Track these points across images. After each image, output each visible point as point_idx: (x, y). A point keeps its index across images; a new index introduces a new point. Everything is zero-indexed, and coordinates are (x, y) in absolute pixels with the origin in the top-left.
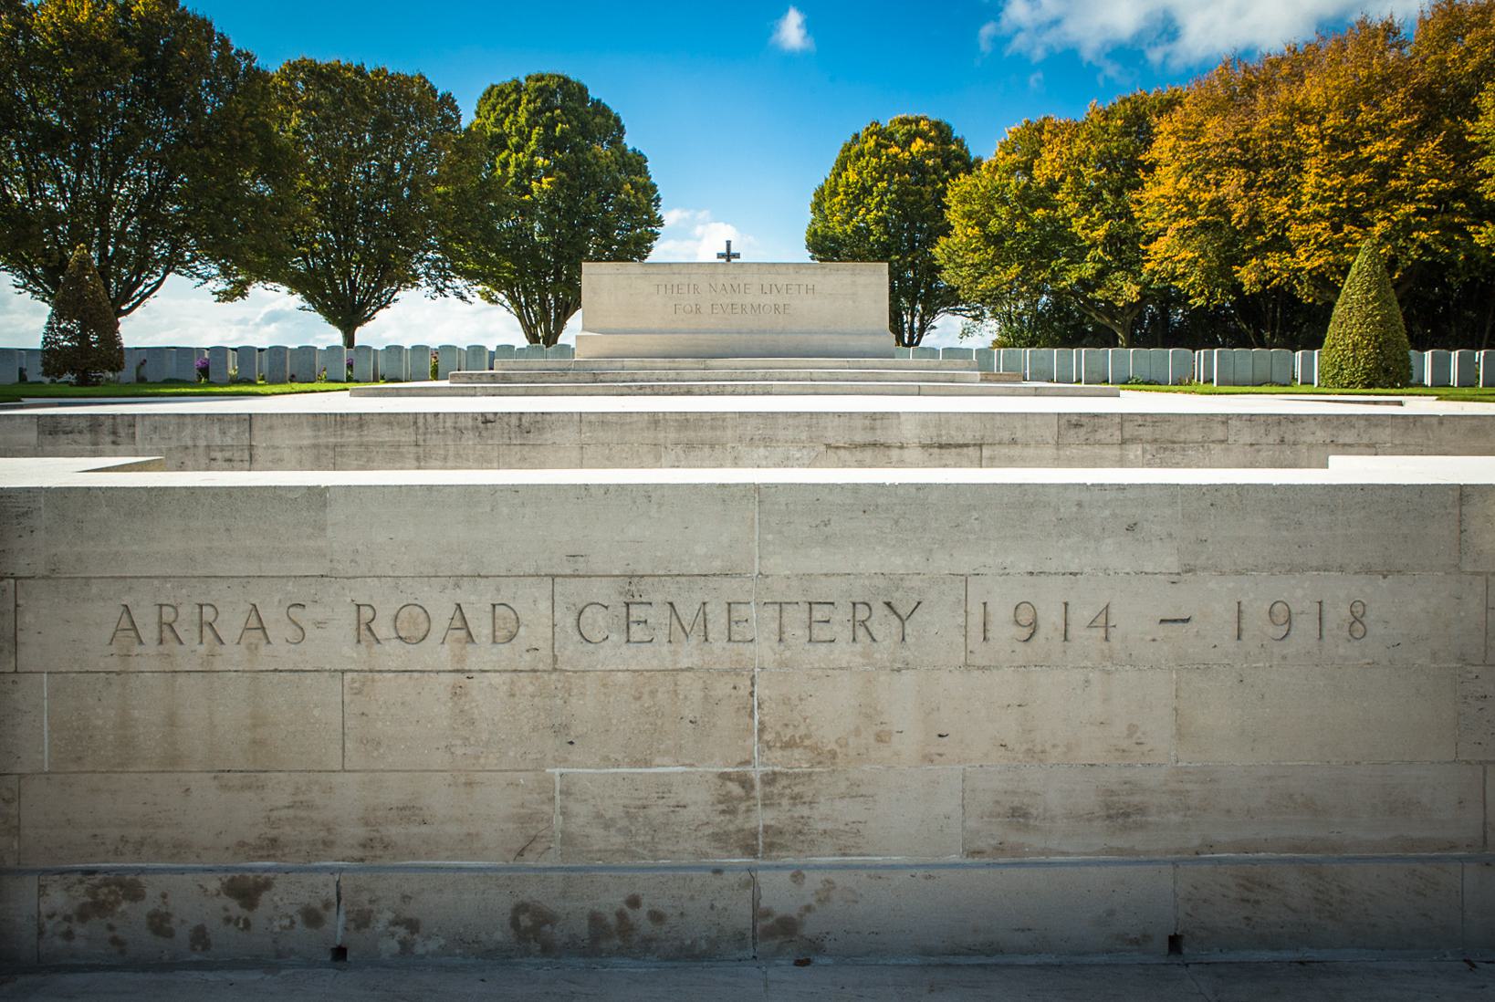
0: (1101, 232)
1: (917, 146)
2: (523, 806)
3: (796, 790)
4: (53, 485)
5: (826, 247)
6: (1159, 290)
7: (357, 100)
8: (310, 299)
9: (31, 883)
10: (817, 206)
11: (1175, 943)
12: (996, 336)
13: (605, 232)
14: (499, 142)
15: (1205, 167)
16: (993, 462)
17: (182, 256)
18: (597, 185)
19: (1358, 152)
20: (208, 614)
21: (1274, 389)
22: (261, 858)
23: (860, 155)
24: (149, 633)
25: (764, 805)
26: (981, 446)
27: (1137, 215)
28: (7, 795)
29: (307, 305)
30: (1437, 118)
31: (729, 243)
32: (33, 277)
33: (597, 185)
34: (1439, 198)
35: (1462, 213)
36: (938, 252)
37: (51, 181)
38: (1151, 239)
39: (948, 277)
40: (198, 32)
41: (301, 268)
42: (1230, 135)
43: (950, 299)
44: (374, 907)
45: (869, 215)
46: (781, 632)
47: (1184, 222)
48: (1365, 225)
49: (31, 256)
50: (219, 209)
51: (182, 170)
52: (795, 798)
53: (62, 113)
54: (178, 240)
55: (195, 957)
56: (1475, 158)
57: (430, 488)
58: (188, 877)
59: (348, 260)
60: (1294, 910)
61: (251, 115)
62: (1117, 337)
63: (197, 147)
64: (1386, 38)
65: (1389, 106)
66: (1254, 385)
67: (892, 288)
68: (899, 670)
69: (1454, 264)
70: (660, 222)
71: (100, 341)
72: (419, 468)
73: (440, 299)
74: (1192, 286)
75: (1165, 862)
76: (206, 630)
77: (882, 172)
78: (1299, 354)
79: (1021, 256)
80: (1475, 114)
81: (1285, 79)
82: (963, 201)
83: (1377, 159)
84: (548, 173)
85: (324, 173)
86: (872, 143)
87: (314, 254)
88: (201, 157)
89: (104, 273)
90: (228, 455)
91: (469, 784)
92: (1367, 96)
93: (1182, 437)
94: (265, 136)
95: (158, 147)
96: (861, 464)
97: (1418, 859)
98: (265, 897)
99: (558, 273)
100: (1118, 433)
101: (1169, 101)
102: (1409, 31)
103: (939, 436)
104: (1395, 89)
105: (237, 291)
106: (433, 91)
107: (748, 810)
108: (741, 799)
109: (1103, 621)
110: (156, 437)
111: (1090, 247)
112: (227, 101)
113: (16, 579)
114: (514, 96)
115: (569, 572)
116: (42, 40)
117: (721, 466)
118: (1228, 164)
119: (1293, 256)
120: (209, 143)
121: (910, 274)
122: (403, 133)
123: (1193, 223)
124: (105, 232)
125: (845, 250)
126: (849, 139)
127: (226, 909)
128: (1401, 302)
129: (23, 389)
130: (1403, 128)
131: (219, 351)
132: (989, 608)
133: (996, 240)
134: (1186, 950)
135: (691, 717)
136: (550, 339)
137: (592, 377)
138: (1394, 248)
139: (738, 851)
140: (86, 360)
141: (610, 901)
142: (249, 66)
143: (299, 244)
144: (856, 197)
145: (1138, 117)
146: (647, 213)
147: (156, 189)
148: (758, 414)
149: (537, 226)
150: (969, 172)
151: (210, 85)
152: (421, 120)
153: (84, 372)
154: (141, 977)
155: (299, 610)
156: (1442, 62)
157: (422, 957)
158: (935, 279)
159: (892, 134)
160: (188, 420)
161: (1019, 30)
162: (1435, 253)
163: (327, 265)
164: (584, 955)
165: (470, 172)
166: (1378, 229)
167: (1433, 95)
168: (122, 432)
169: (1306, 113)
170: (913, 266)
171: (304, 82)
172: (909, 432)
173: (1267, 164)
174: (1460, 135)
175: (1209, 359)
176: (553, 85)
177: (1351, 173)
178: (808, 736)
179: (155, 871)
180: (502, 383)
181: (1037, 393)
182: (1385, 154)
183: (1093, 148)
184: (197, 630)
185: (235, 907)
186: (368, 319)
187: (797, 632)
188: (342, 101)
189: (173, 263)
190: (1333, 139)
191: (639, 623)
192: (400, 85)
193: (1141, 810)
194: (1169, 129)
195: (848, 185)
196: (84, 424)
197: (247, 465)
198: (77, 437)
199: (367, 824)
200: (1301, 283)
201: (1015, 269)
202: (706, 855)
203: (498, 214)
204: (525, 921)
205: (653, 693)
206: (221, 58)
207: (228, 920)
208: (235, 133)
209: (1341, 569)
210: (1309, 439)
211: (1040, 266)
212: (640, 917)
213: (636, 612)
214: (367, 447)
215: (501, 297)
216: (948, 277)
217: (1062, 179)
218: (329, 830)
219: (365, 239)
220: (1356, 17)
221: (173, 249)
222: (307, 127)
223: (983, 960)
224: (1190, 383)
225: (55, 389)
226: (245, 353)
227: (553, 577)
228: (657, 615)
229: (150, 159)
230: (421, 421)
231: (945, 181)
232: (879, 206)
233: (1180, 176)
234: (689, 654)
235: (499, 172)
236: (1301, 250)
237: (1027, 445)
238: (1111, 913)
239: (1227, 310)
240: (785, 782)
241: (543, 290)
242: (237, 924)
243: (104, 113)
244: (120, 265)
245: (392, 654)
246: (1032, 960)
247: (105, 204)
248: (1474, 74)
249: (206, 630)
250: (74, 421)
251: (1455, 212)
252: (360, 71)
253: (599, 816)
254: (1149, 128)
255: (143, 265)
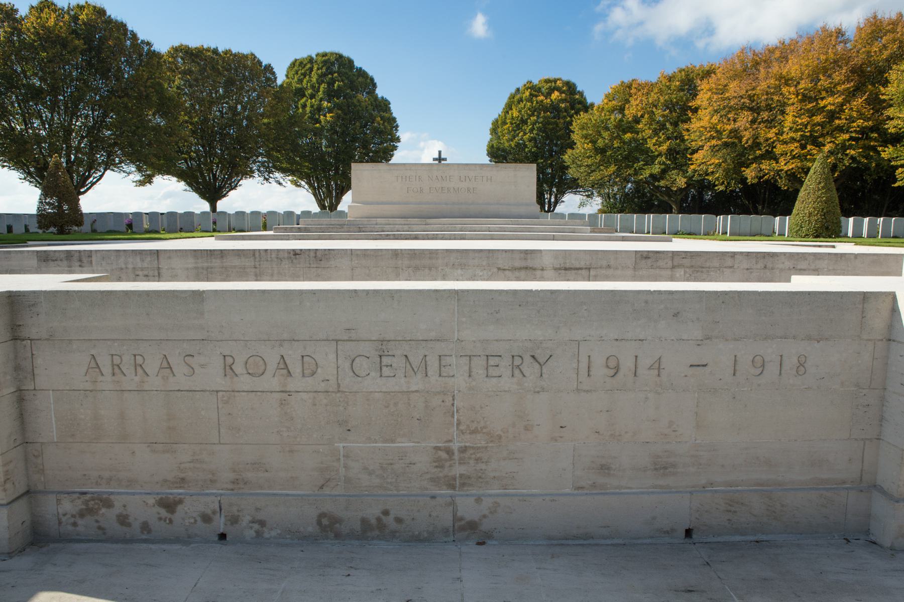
0: (664, 148)
1: (555, 95)
2: (322, 463)
3: (478, 456)
4: (44, 289)
5: (498, 154)
6: (698, 181)
7: (214, 68)
8: (189, 184)
9: (52, 498)
10: (494, 131)
11: (688, 533)
12: (600, 207)
13: (365, 145)
14: (300, 93)
15: (727, 110)
16: (596, 278)
17: (114, 161)
18: (360, 118)
19: (818, 103)
20: (139, 360)
21: (762, 238)
22: (177, 488)
23: (521, 100)
24: (107, 369)
25: (460, 463)
26: (589, 269)
27: (686, 137)
28: (36, 454)
29: (188, 188)
30: (864, 85)
31: (440, 152)
32: (29, 173)
33: (360, 118)
34: (864, 131)
35: (875, 140)
36: (567, 157)
37: (37, 118)
38: (695, 152)
39: (572, 173)
40: (118, 30)
41: (184, 166)
42: (744, 92)
43: (573, 186)
44: (240, 514)
45: (525, 136)
46: (470, 371)
47: (714, 142)
48: (820, 145)
49: (27, 161)
50: (134, 133)
51: (112, 111)
52: (477, 460)
53: (41, 79)
54: (111, 152)
55: (144, 537)
56: (885, 108)
57: (264, 291)
58: (136, 497)
59: (212, 162)
60: (755, 516)
61: (151, 78)
62: (671, 208)
63: (120, 97)
64: (837, 37)
65: (837, 77)
66: (751, 235)
67: (538, 179)
68: (538, 392)
69: (869, 169)
70: (398, 140)
71: (69, 209)
72: (257, 280)
73: (266, 184)
74: (717, 179)
75: (686, 492)
76: (139, 369)
77: (533, 111)
78: (778, 218)
79: (616, 161)
80: (885, 83)
81: (777, 60)
82: (583, 128)
83: (829, 108)
84: (330, 111)
85: (196, 112)
86: (527, 94)
87: (191, 159)
88: (122, 103)
89: (69, 171)
90: (146, 273)
91: (291, 451)
92: (825, 70)
93: (708, 264)
94: (160, 91)
95: (98, 98)
96: (518, 279)
97: (824, 489)
98: (179, 508)
99: (337, 169)
100: (670, 262)
101: (708, 71)
102: (851, 33)
103: (565, 263)
104: (841, 67)
105: (147, 180)
106: (260, 63)
107: (451, 466)
108: (446, 460)
109: (658, 366)
110: (104, 263)
111: (658, 156)
112: (137, 70)
113: (31, 340)
114: (309, 66)
115: (346, 338)
116: (28, 37)
117: (435, 280)
118: (742, 109)
119: (777, 163)
120: (127, 95)
121: (549, 171)
122: (242, 88)
123: (720, 142)
124: (69, 147)
125: (511, 157)
126: (513, 91)
127: (159, 513)
128: (837, 190)
129: (27, 236)
130: (845, 90)
131: (138, 215)
132: (591, 359)
133: (602, 151)
134: (694, 536)
135: (418, 417)
136: (333, 207)
137: (358, 229)
138: (836, 159)
139: (445, 487)
140: (62, 219)
141: (373, 512)
142: (149, 50)
143: (182, 153)
144: (518, 126)
145: (689, 80)
146: (390, 134)
147: (97, 122)
148: (458, 251)
149: (324, 142)
150: (586, 111)
151: (127, 61)
152: (253, 80)
153: (61, 226)
154: (115, 546)
155: (190, 358)
156: (869, 52)
157: (268, 539)
158: (564, 174)
159: (540, 88)
160: (122, 253)
161: (618, 27)
162: (859, 162)
163: (199, 165)
164: (358, 539)
165: (283, 111)
166: (827, 148)
167: (862, 72)
168: (85, 260)
169: (789, 80)
170: (551, 166)
171: (182, 59)
172: (547, 261)
173: (765, 109)
174: (877, 95)
175: (725, 221)
176: (333, 59)
177: (813, 115)
178: (485, 427)
179: (119, 493)
180: (304, 233)
181: (624, 239)
182: (833, 104)
183: (661, 98)
184: (133, 368)
185: (163, 513)
186: (224, 196)
187: (479, 371)
188: (205, 69)
189: (109, 165)
190: (804, 95)
191: (387, 366)
192: (240, 59)
193: (674, 466)
194: (707, 87)
195: (513, 118)
196: (63, 256)
197: (157, 278)
198: (59, 263)
199: (234, 471)
200: (781, 178)
201: (613, 168)
202: (427, 489)
203: (300, 135)
204: (325, 522)
205: (396, 404)
206: (133, 45)
207: (160, 519)
208: (142, 89)
209: (794, 337)
210: (781, 266)
211: (628, 167)
212: (389, 520)
213: (385, 360)
214: (226, 268)
215: (303, 183)
216: (572, 173)
217: (642, 116)
218: (213, 474)
219: (221, 150)
220: (819, 25)
221: (109, 156)
222: (184, 85)
223: (581, 542)
224: (713, 234)
225: (45, 236)
226: (153, 216)
227: (337, 341)
228: (399, 362)
229: (93, 106)
230: (257, 255)
231: (571, 116)
232: (531, 131)
233: (713, 115)
234: (417, 383)
235: (301, 110)
236: (782, 159)
237: (617, 268)
238: (654, 518)
239: (737, 193)
240: (472, 451)
241: (328, 179)
242: (165, 521)
243: (65, 78)
244: (79, 166)
245: (245, 382)
246: (609, 542)
247: (68, 131)
248: (887, 60)
249: (139, 369)
250: (57, 254)
251: (871, 139)
252: (215, 51)
253: (365, 468)
254: (695, 87)
255: (92, 166)
